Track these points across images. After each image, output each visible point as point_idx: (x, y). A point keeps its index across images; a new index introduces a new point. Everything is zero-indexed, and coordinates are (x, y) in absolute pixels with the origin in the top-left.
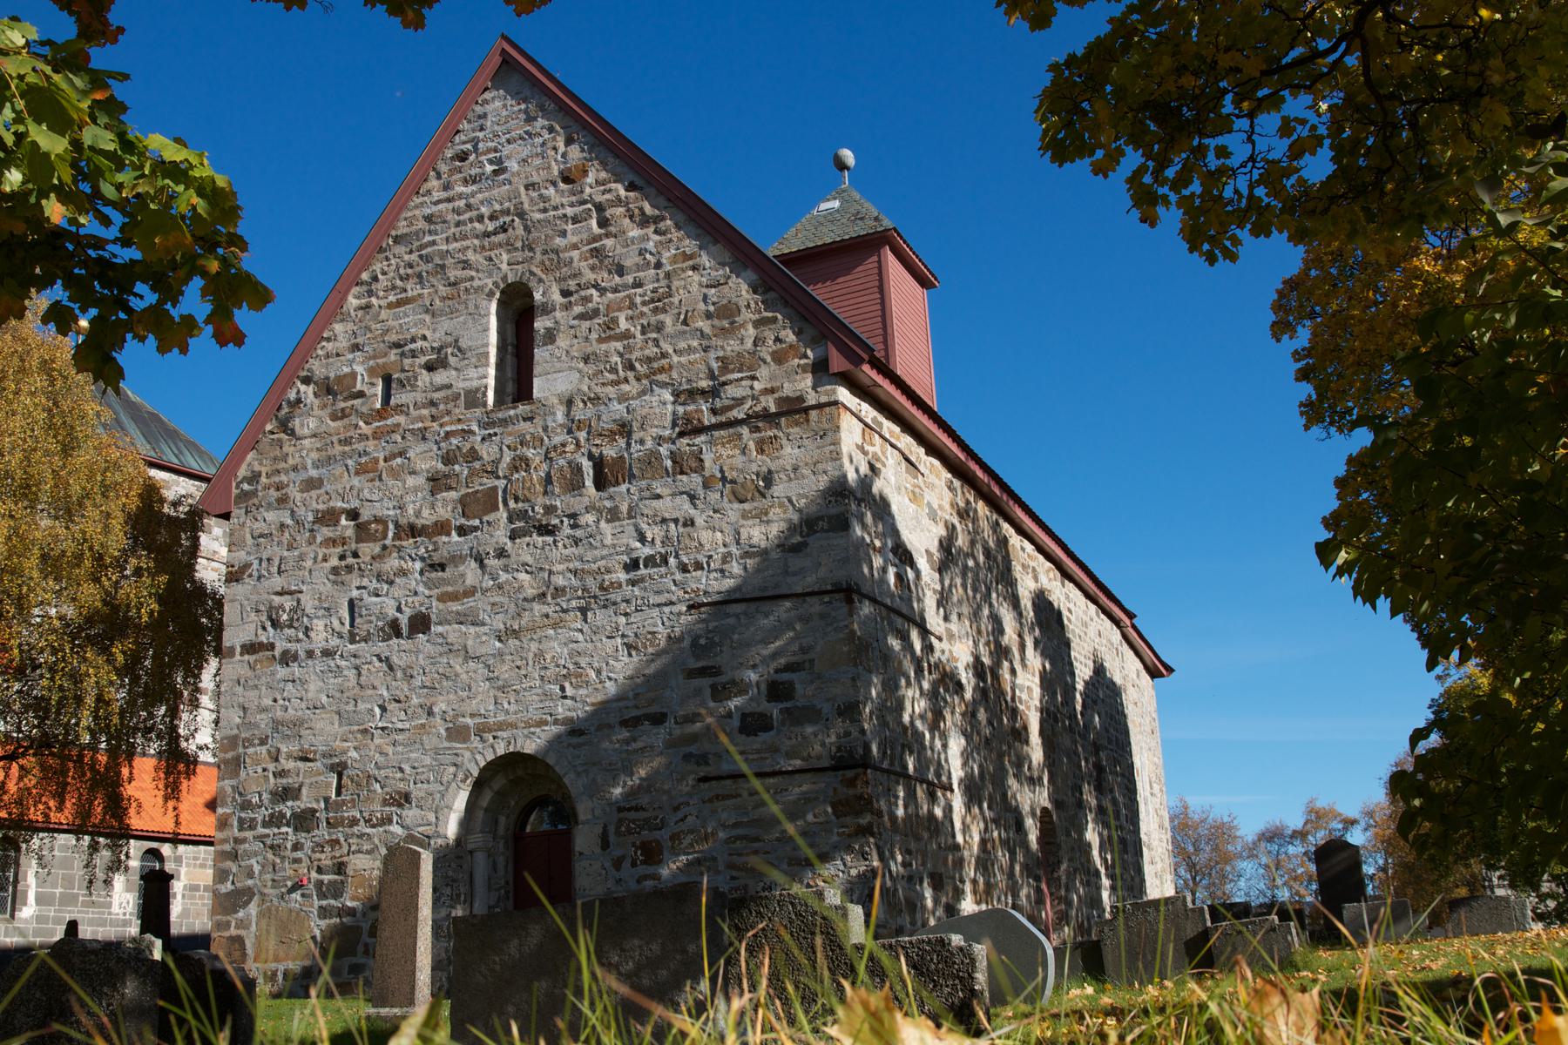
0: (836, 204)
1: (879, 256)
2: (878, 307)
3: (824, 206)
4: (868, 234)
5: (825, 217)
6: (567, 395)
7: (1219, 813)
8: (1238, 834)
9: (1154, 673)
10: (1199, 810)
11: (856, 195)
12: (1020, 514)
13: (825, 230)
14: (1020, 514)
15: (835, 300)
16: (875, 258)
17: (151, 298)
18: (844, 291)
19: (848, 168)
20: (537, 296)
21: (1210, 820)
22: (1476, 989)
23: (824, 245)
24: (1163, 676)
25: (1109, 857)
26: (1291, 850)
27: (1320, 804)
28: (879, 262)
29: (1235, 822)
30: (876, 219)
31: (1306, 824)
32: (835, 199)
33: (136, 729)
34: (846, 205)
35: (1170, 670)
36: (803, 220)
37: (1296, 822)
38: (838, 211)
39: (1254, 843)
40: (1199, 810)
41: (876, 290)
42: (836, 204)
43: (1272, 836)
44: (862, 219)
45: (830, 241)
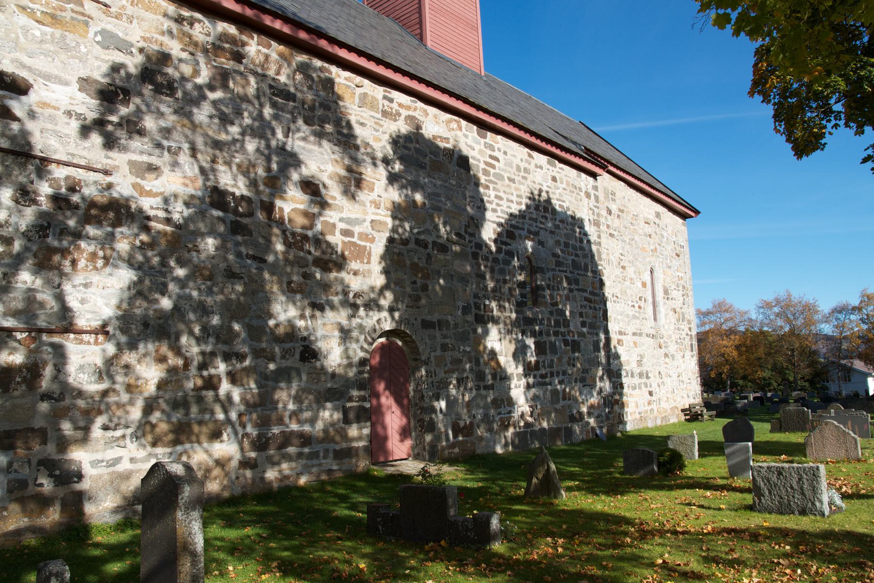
7: (809, 298)
8: (819, 309)
9: (684, 216)
10: (797, 297)
12: (343, 54)
14: (343, 54)
17: (353, 431)
21: (803, 302)
24: (692, 217)
25: (332, 500)
26: (852, 317)
27: (869, 292)
29: (817, 303)
31: (861, 302)
33: (487, 567)
35: (697, 212)
37: (856, 302)
39: (830, 314)
40: (797, 297)
43: (841, 310)
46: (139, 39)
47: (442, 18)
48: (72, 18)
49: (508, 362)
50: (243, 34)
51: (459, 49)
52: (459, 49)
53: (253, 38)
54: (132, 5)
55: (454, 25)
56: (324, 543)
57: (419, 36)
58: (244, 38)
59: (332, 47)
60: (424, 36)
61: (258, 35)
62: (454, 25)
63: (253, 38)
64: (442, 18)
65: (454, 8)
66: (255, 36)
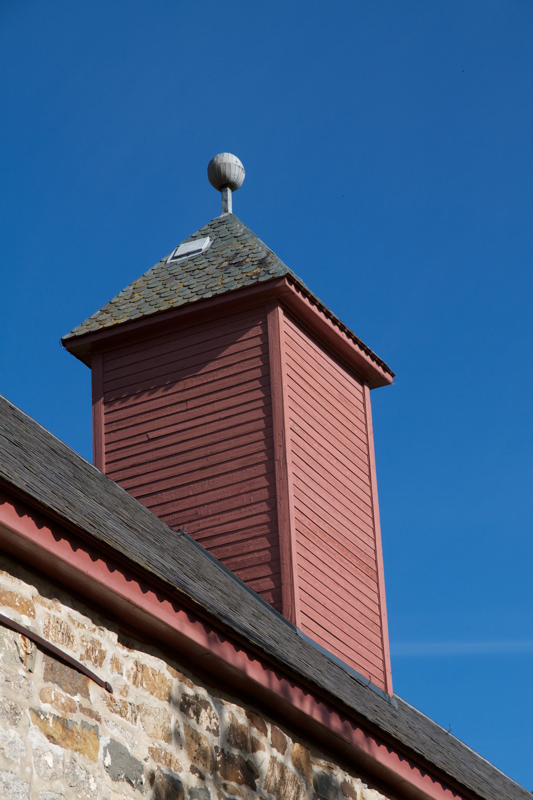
0: (205, 243)
1: (265, 326)
2: (260, 414)
3: (184, 248)
4: (244, 288)
5: (182, 265)
6: (81, 641)
11: (240, 228)
13: (177, 285)
15: (191, 404)
16: (257, 330)
18: (206, 389)
19: (233, 186)
20: (244, 780)
22: (393, 697)
23: (172, 310)
28: (265, 336)
30: (262, 263)
32: (205, 235)
34: (220, 243)
36: (149, 273)
38: (205, 254)
41: (257, 384)
42: (205, 243)
44: (239, 264)
45: (181, 302)
46: (146, 753)
47: (318, 553)
48: (84, 725)
49: (187, 776)
50: (255, 725)
51: (347, 629)
52: (347, 629)
53: (264, 731)
54: (134, 683)
55: (337, 568)
56: (112, 709)
57: (269, 595)
58: (255, 732)
59: (369, 743)
60: (286, 600)
61: (273, 724)
62: (337, 568)
63: (264, 731)
64: (318, 553)
65: (335, 524)
66: (269, 727)
